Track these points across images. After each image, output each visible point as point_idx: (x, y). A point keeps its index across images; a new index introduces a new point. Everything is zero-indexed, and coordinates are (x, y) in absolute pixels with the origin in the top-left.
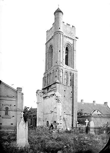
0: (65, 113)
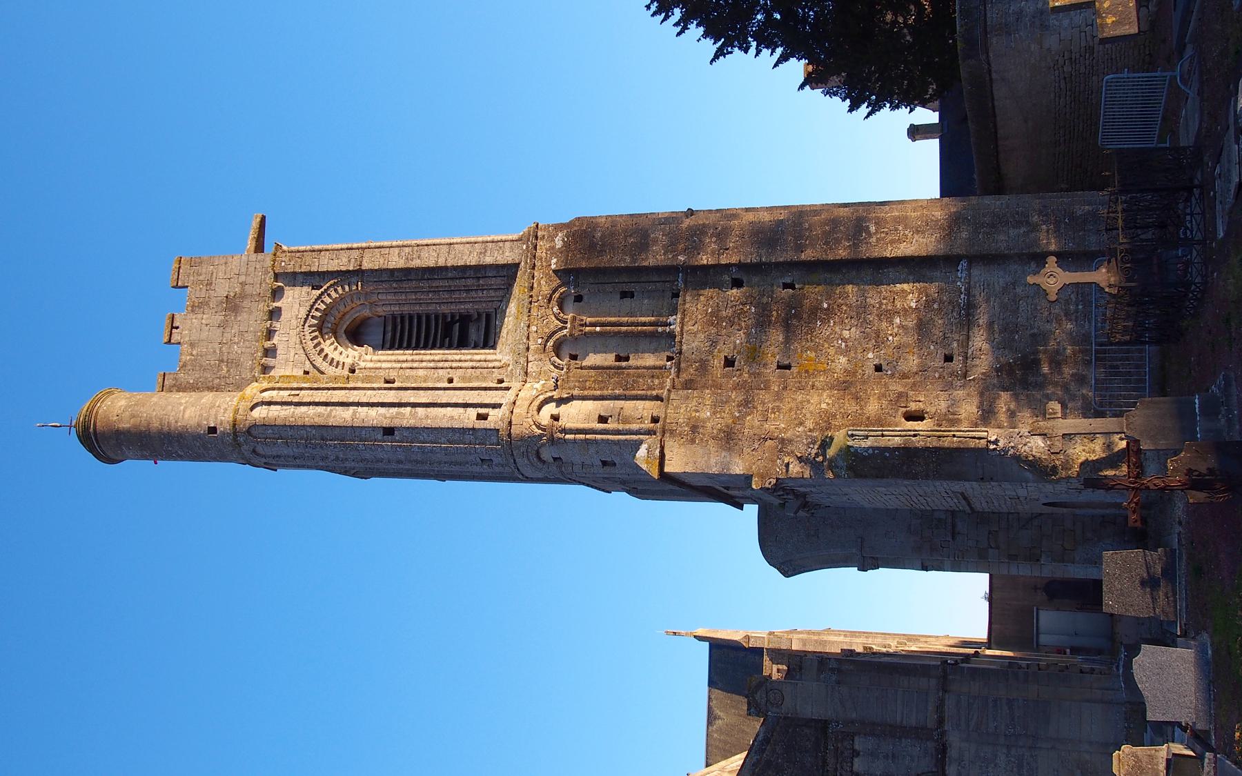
0: (948, 358)
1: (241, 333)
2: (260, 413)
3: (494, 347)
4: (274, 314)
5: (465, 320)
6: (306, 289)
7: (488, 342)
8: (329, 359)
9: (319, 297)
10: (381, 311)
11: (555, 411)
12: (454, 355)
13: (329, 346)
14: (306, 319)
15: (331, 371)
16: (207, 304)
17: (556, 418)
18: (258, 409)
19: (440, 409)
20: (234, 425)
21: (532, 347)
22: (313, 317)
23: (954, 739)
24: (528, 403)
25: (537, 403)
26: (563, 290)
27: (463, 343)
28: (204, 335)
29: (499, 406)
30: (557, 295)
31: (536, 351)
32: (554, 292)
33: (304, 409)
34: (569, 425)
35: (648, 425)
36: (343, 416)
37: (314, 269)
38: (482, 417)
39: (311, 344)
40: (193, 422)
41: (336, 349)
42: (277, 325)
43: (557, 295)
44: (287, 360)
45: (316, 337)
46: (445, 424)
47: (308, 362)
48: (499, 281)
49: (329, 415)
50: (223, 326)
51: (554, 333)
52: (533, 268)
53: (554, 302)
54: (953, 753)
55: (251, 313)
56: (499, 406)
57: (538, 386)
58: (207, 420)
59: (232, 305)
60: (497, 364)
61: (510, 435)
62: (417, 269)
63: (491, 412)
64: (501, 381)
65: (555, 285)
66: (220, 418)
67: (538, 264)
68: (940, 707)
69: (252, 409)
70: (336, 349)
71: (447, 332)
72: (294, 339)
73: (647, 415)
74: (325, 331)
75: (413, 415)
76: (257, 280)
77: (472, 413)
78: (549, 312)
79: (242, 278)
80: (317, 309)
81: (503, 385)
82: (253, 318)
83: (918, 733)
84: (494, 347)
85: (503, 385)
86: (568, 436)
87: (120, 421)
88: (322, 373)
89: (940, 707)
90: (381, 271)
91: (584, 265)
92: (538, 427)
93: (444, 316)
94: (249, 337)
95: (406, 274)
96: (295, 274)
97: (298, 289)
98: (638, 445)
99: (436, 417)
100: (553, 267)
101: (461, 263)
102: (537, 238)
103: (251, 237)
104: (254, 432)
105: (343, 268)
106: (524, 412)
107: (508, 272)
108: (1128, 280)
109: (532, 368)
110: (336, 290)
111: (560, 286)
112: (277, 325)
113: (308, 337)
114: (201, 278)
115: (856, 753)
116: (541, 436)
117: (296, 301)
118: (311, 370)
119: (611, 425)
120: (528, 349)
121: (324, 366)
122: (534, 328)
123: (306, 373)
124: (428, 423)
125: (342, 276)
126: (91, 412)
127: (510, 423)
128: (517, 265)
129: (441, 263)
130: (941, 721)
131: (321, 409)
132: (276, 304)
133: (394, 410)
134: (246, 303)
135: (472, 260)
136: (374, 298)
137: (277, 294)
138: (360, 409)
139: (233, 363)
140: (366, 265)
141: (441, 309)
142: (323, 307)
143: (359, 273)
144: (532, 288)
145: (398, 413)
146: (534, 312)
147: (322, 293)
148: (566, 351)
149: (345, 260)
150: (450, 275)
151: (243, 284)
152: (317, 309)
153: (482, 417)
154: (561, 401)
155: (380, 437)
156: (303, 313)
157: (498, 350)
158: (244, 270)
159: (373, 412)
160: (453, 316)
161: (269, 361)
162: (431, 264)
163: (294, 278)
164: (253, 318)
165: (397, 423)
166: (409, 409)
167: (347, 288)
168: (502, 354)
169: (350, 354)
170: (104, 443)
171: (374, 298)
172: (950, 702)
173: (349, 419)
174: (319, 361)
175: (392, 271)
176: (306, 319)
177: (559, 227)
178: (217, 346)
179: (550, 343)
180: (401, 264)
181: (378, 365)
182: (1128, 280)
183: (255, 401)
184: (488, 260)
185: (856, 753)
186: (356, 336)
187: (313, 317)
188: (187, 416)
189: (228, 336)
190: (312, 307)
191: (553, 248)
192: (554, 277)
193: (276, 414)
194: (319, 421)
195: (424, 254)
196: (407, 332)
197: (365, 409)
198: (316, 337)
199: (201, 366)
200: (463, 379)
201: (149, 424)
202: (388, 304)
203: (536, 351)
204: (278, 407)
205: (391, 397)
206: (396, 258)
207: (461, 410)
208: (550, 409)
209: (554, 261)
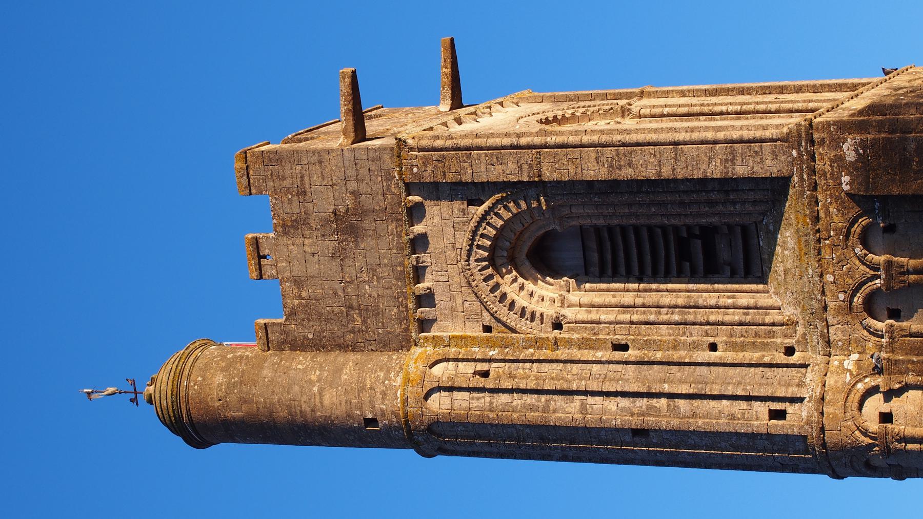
1: (372, 269)
2: (439, 404)
3: (762, 279)
4: (419, 243)
5: (708, 234)
6: (458, 205)
7: (752, 267)
8: (508, 302)
9: (483, 218)
11: (885, 408)
12: (709, 294)
13: (510, 284)
14: (469, 252)
15: (523, 325)
16: (306, 222)
17: (886, 418)
18: (436, 396)
19: (713, 403)
20: (407, 422)
21: (831, 305)
22: (479, 247)
24: (843, 395)
25: (855, 397)
26: (864, 221)
27: (710, 270)
28: (313, 269)
29: (801, 400)
30: (856, 229)
31: (838, 311)
32: (852, 224)
33: (504, 398)
34: (910, 431)
37: (467, 178)
38: (779, 415)
39: (485, 288)
40: (340, 411)
41: (522, 288)
42: (426, 258)
43: (856, 229)
44: (453, 310)
45: (490, 277)
46: (723, 425)
47: (485, 314)
48: (759, 196)
49: (546, 409)
50: (339, 255)
51: (862, 284)
52: (815, 188)
53: (854, 239)
55: (379, 237)
56: (801, 400)
57: (850, 363)
58: (360, 409)
59: (347, 225)
60: (773, 316)
61: (824, 445)
63: (790, 409)
64: (790, 351)
65: (852, 214)
66: (380, 406)
67: (822, 182)
69: (427, 396)
70: (515, 280)
71: (684, 254)
72: (457, 280)
74: (499, 261)
75: (674, 412)
76: (377, 188)
77: (762, 409)
78: (849, 253)
79: (352, 186)
80: (482, 236)
81: (793, 359)
82: (383, 243)
84: (762, 279)
85: (793, 359)
86: (910, 446)
87: (227, 406)
88: (513, 331)
90: (572, 183)
91: (895, 191)
92: (865, 433)
93: (676, 228)
94: (385, 272)
95: (611, 187)
96: (436, 185)
97: (445, 204)
99: (708, 416)
100: (846, 188)
101: (698, 175)
102: (812, 142)
103: (343, 109)
104: (435, 428)
105: (513, 178)
106: (839, 412)
107: (775, 190)
109: (835, 334)
110: (506, 207)
111: (860, 216)
112: (426, 258)
113: (479, 277)
114: (286, 183)
116: (870, 447)
117: (445, 223)
118: (494, 324)
120: (825, 308)
121: (512, 319)
122: (829, 278)
123: (487, 329)
124: (700, 424)
125: (513, 190)
126: (178, 388)
127: (822, 430)
129: (666, 172)
131: (530, 399)
132: (418, 229)
133: (643, 403)
134: (368, 223)
135: (715, 170)
136: (566, 211)
137: (415, 213)
138: (590, 400)
139: (370, 311)
140: (548, 175)
142: (492, 232)
143: (538, 186)
144: (817, 219)
145: (650, 408)
146: (827, 255)
147: (487, 213)
148: (881, 307)
149: (512, 166)
150: (682, 187)
151: (355, 194)
152: (482, 236)
154: (889, 395)
155: (628, 438)
156: (463, 241)
157: (771, 287)
158: (351, 172)
159: (612, 404)
160: (689, 228)
161: (425, 312)
162: (650, 173)
163: (437, 191)
164: (382, 247)
165: (651, 421)
166: (664, 401)
167: (523, 205)
168: (776, 298)
169: (545, 295)
170: (198, 428)
171: (566, 211)
173: (578, 416)
174: (502, 312)
175: (590, 184)
176: (469, 252)
177: (845, 127)
178: (339, 287)
179: (858, 300)
181: (594, 315)
183: (428, 386)
184: (741, 170)
186: (543, 261)
187: (479, 247)
188: (327, 400)
189: (350, 272)
190: (474, 233)
191: (840, 158)
192: (849, 203)
193: (465, 404)
194: (533, 417)
195: (638, 160)
197: (598, 399)
198: (490, 277)
199: (320, 315)
201: (271, 413)
202: (586, 215)
203: (838, 311)
204: (466, 395)
205: (631, 378)
206: (593, 165)
207: (744, 405)
208: (875, 405)
209: (846, 179)
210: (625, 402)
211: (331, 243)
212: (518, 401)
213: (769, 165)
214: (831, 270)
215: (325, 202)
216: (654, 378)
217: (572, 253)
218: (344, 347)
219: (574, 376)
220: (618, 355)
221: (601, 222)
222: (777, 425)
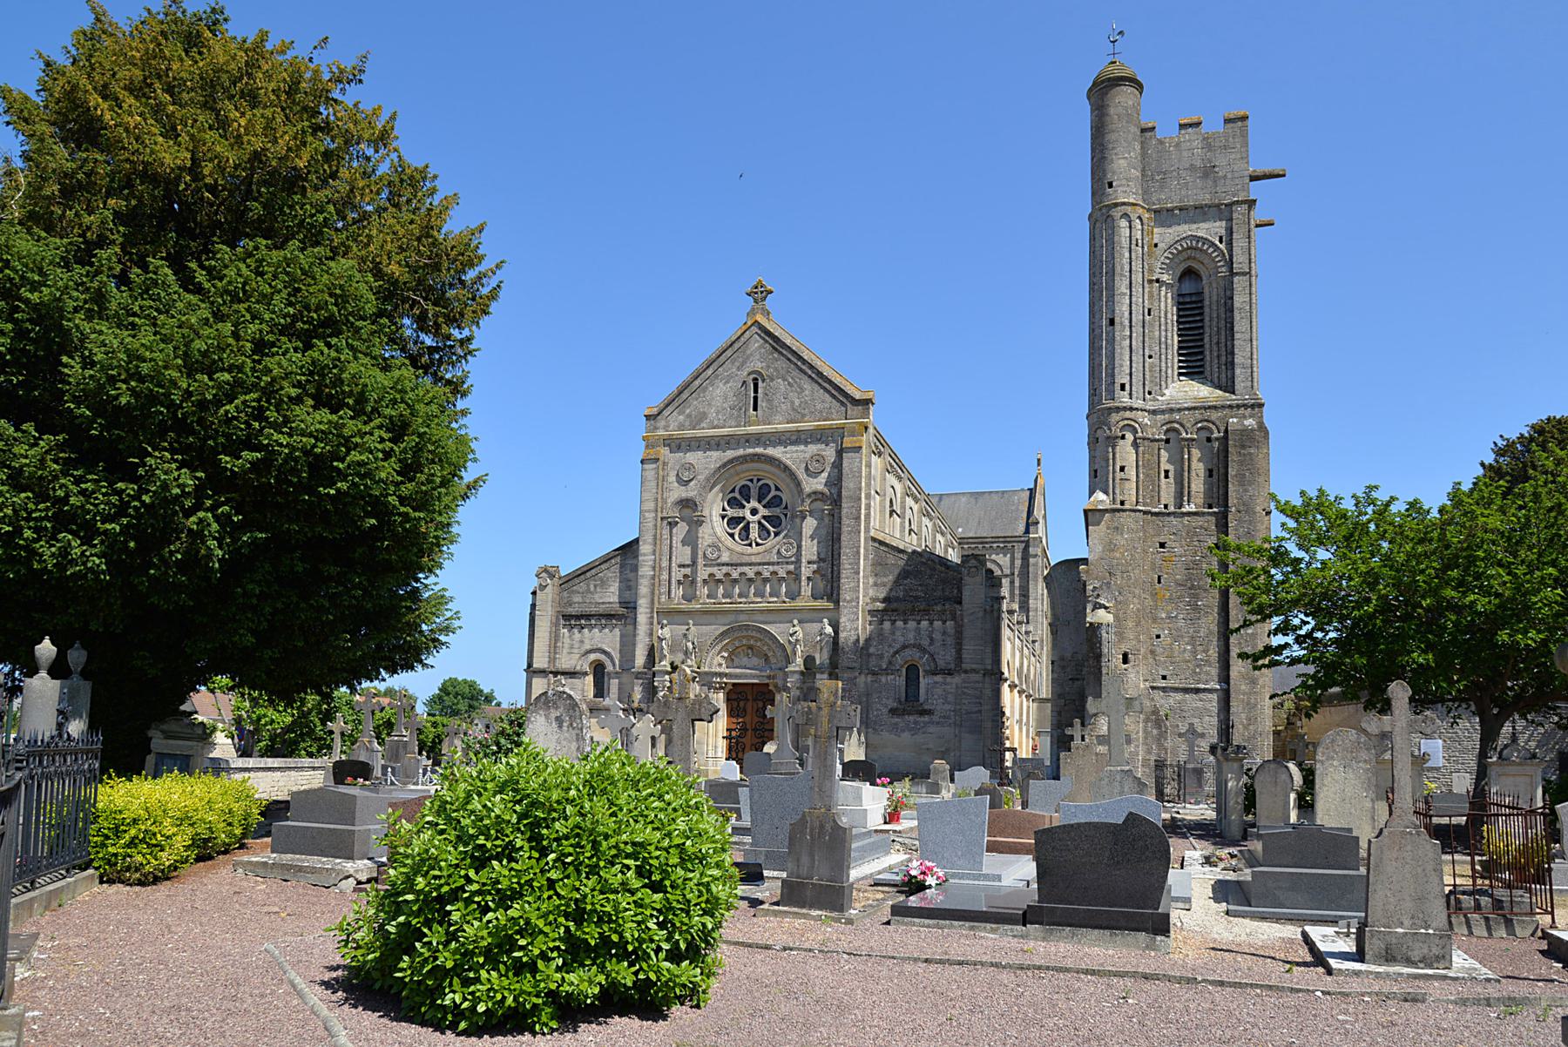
0: (1164, 678)
10: (1206, 291)
23: (956, 680)
28: (1185, 154)
35: (1119, 498)
36: (1122, 286)
38: (1123, 387)
50: (1192, 168)
54: (949, 679)
59: (1208, 171)
62: (1232, 317)
63: (1126, 393)
68: (975, 671)
73: (1126, 497)
77: (1126, 380)
83: (959, 658)
89: (975, 671)
98: (1106, 493)
108: (1358, 698)
115: (944, 622)
119: (1119, 475)
128: (1233, 393)
129: (1237, 336)
130: (966, 672)
131: (1127, 268)
133: (1127, 323)
141: (1206, 337)
153: (1123, 387)
159: (1126, 308)
172: (978, 677)
180: (1236, 305)
182: (1358, 698)
184: (1238, 371)
185: (944, 622)
196: (1190, 312)
200: (1152, 366)
202: (1211, 294)
205: (1137, 318)
210: (1127, 314)
211: (1198, 163)
212: (1126, 261)
213: (1239, 386)
214: (279, 605)
215: (1221, 161)
216: (1138, 329)
217: (1188, 287)
218: (1143, 170)
219: (1137, 290)
220: (1149, 309)
221: (1207, 303)
222: (1117, 387)
